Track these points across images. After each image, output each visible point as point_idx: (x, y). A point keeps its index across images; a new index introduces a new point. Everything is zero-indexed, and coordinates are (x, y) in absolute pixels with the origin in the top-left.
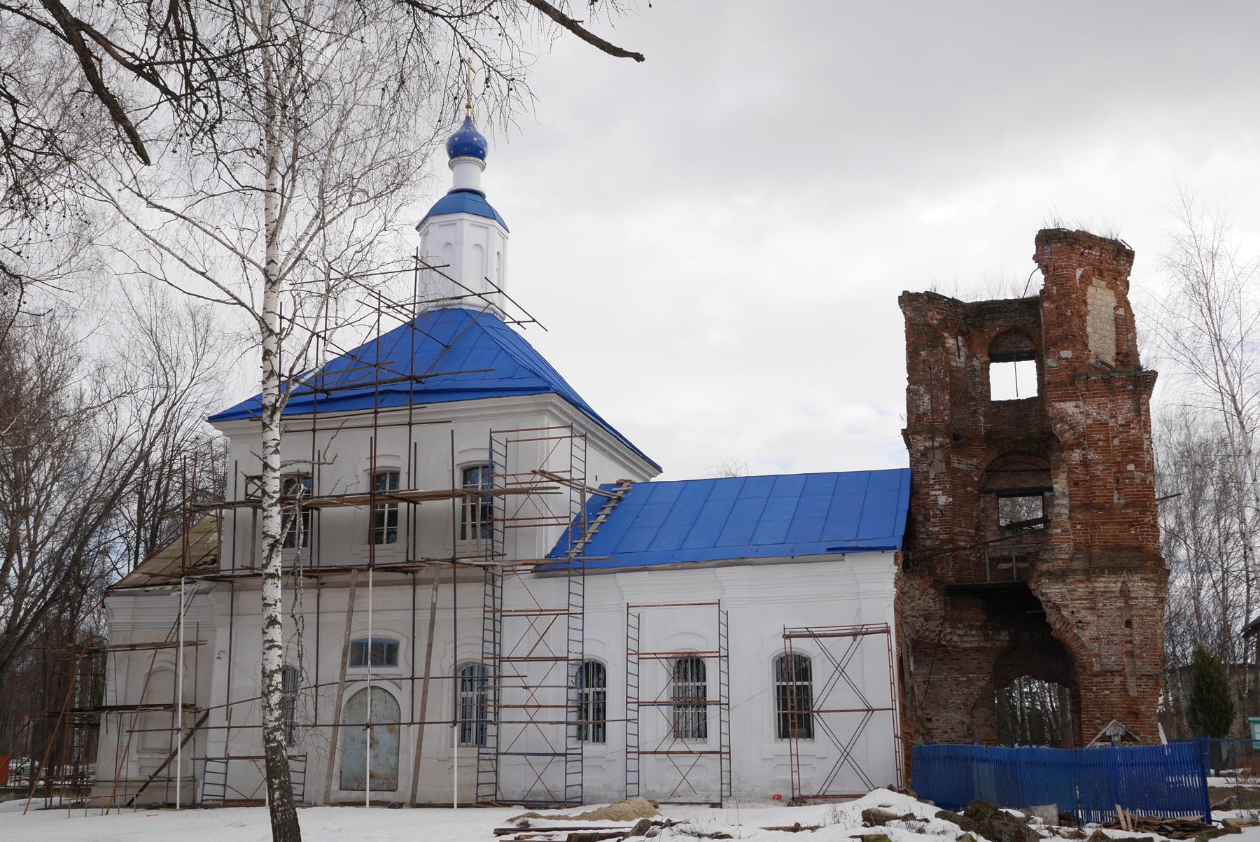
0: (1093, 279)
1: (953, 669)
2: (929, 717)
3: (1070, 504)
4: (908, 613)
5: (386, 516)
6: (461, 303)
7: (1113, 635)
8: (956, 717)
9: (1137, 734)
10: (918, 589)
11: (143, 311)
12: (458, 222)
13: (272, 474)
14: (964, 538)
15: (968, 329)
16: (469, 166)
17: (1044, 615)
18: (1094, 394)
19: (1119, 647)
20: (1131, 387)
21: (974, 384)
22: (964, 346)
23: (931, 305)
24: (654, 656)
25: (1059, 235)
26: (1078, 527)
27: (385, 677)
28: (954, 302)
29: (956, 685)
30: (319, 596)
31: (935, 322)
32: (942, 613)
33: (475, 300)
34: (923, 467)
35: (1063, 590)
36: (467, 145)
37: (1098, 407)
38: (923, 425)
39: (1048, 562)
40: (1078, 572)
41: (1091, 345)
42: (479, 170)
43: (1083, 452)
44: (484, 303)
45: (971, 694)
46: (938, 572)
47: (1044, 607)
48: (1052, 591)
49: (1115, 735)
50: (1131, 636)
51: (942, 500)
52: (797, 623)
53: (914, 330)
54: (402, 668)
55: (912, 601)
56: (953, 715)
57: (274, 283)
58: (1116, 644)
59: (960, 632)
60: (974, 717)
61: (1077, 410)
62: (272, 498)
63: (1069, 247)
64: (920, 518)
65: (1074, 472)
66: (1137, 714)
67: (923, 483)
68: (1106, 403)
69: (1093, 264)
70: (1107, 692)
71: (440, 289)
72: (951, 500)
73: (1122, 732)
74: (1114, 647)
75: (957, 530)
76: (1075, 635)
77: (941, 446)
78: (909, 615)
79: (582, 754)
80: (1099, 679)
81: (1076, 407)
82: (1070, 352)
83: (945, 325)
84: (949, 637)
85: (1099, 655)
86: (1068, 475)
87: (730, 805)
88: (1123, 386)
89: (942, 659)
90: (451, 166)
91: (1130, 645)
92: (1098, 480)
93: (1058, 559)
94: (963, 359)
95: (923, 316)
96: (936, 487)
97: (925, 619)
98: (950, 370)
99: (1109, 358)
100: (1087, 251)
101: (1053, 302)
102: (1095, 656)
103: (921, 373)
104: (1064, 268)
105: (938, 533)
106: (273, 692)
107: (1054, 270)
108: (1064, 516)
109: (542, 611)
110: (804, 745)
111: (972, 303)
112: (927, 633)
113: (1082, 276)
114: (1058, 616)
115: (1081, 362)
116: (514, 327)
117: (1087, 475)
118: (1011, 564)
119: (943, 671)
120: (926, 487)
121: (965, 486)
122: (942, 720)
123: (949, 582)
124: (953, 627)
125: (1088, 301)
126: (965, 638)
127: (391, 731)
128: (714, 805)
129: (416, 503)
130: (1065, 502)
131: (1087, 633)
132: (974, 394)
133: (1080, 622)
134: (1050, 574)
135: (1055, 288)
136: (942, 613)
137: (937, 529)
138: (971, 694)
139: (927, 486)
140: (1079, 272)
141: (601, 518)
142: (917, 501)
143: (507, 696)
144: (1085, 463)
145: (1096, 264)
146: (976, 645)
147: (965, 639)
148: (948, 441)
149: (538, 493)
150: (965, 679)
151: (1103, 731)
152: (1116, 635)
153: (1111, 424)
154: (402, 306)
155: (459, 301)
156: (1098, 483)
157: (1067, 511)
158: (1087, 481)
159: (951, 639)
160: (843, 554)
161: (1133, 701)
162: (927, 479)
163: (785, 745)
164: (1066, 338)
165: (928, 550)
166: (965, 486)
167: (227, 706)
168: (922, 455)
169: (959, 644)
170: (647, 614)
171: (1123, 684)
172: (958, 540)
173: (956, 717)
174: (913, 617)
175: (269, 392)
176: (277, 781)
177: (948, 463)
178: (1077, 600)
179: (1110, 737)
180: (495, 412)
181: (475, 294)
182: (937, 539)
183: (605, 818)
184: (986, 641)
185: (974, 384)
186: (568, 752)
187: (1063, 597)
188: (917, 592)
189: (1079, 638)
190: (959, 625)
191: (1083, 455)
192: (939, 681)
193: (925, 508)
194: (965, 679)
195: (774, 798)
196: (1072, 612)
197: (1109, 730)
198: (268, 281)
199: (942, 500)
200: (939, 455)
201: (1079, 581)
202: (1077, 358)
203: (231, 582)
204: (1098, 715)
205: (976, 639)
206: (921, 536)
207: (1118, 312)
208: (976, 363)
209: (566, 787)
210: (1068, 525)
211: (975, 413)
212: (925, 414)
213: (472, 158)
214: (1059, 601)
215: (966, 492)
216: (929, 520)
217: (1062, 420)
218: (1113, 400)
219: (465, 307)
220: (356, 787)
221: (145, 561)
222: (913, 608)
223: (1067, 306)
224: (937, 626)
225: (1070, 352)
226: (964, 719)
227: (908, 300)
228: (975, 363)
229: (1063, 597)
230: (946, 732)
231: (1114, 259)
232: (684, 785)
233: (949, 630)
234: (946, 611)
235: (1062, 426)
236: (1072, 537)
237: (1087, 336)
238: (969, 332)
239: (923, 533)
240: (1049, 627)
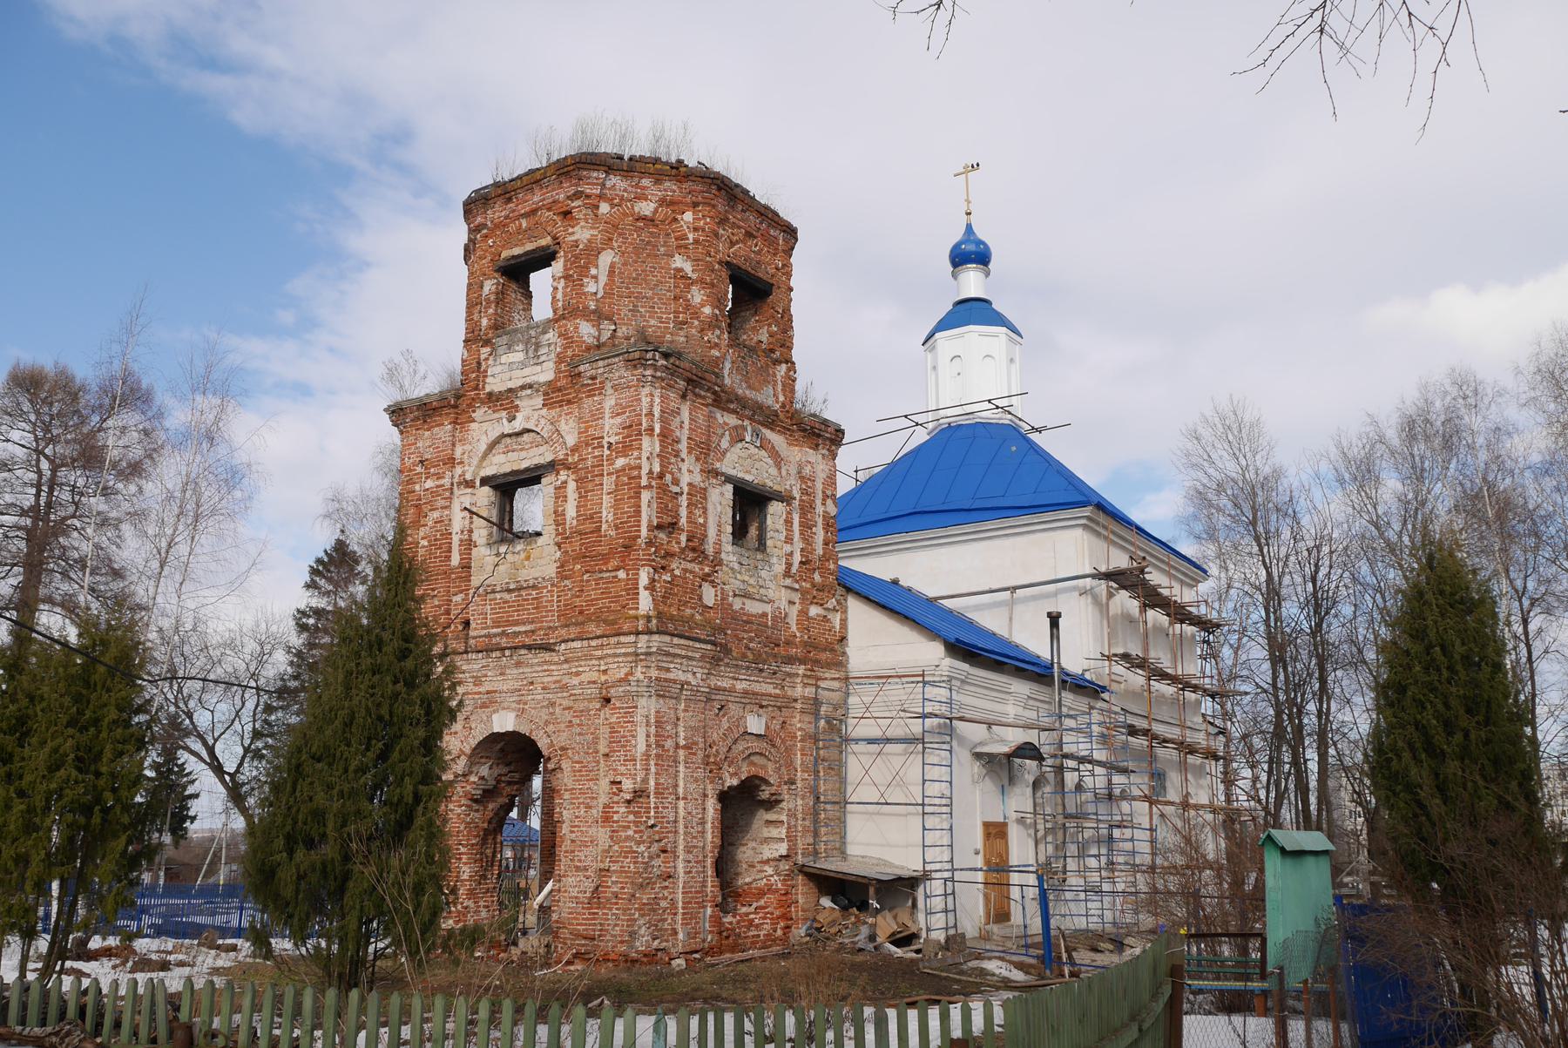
90: (954, 276)
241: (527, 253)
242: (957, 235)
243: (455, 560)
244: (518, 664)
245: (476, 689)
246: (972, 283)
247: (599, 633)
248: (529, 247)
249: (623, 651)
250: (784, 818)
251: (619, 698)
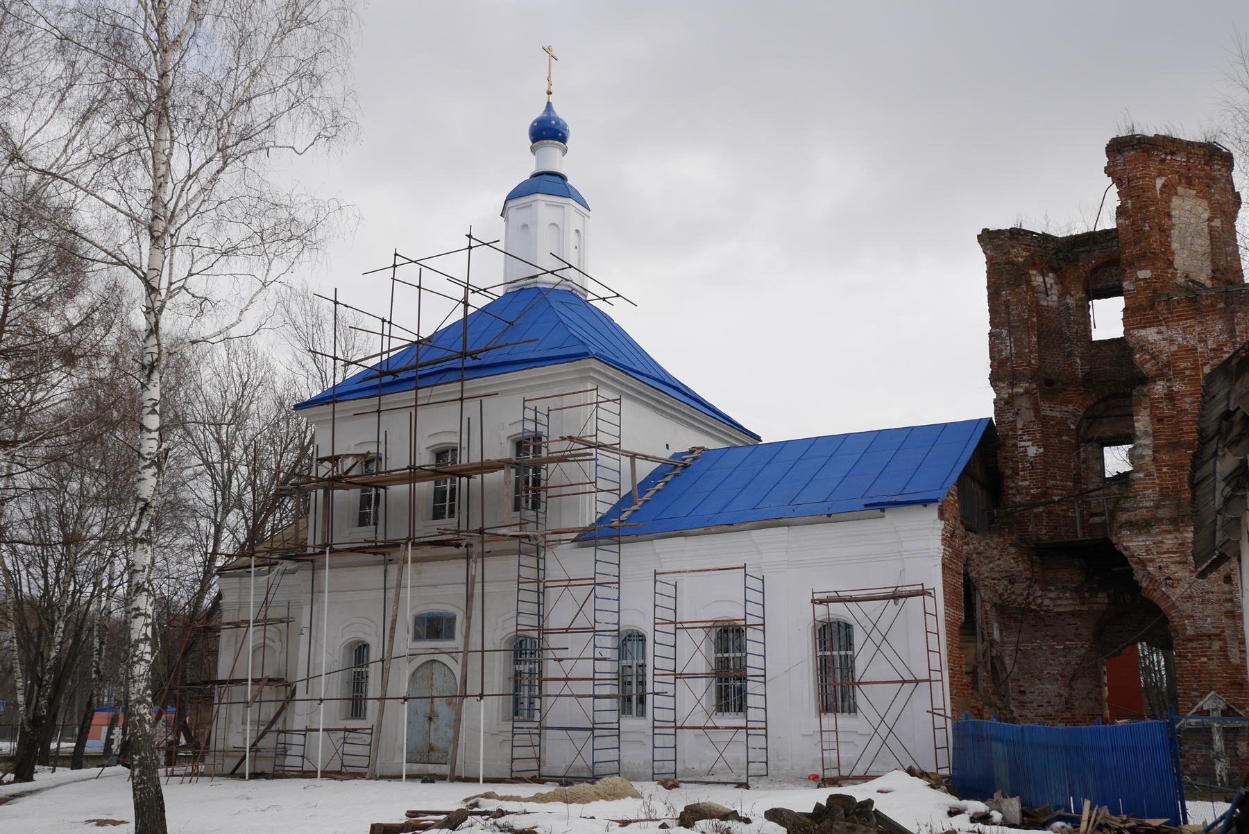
0: (1179, 188)
1: (1047, 636)
2: (1022, 689)
3: (1154, 444)
4: (986, 575)
5: (448, 492)
6: (536, 282)
7: (1208, 593)
8: (1052, 689)
9: (1241, 707)
10: (996, 548)
11: (300, 321)
12: (533, 203)
13: (147, 435)
14: (1060, 492)
15: (1059, 265)
17: (1131, 572)
18: (1177, 316)
19: (1216, 606)
20: (1222, 305)
21: (1068, 324)
22: (1056, 283)
23: (1015, 241)
24: (685, 625)
25: (1132, 141)
26: (1165, 469)
27: (444, 650)
28: (1045, 237)
29: (1052, 654)
30: (386, 571)
31: (1020, 259)
32: (1028, 574)
33: (548, 278)
34: (1009, 416)
35: (1147, 543)
36: (545, 129)
37: (1184, 332)
38: (1007, 371)
39: (1129, 511)
40: (1164, 521)
41: (1178, 262)
42: (561, 153)
43: (1168, 384)
44: (558, 280)
45: (1069, 663)
46: (1030, 530)
47: (1131, 563)
48: (1134, 544)
49: (1214, 710)
50: (1231, 593)
51: (1032, 451)
52: (827, 586)
53: (995, 269)
54: (458, 643)
55: (991, 562)
56: (1050, 687)
57: (158, 238)
58: (1212, 604)
59: (1052, 595)
60: (1074, 690)
61: (1160, 337)
62: (145, 459)
63: (1145, 154)
64: (1008, 472)
65: (1157, 407)
66: (1242, 685)
67: (1010, 433)
68: (1194, 326)
69: (1178, 172)
70: (1205, 659)
71: (522, 271)
72: (1041, 450)
73: (1222, 706)
74: (1210, 607)
75: (1050, 483)
76: (1164, 593)
77: (1027, 392)
78: (987, 577)
79: (619, 729)
80: (1195, 644)
81: (1158, 333)
82: (1149, 271)
83: (1032, 263)
84: (1039, 601)
85: (1192, 617)
86: (1151, 410)
87: (760, 785)
88: (1212, 305)
89: (1035, 626)
90: (533, 150)
91: (1230, 604)
92: (1186, 414)
93: (1141, 508)
94: (1055, 298)
95: (1005, 254)
96: (1026, 437)
97: (1010, 580)
98: (1038, 310)
99: (1204, 277)
100: (1169, 157)
101: (1128, 218)
102: (1189, 617)
103: (1003, 315)
104: (1140, 178)
105: (1028, 488)
106: (137, 662)
107: (1129, 181)
108: (1147, 458)
109: (570, 580)
110: (844, 721)
111: (1067, 237)
112: (1013, 597)
113: (1164, 185)
114: (1145, 573)
115: (1162, 282)
116: (599, 304)
117: (1174, 409)
118: (1103, 518)
119: (1036, 639)
120: (1013, 438)
121: (1059, 435)
122: (1037, 693)
123: (999, 538)
124: (1043, 589)
125: (1173, 213)
126: (1057, 601)
127: (449, 704)
128: (740, 785)
129: (469, 477)
130: (1148, 442)
131: (1178, 591)
132: (1068, 334)
133: (1170, 579)
134: (1131, 525)
135: (1130, 201)
136: (1028, 574)
137: (1026, 483)
138: (1069, 663)
139: (1015, 437)
140: (1159, 183)
141: (659, 486)
142: (1004, 454)
143: (552, 669)
144: (1171, 396)
145: (1183, 171)
146: (1069, 609)
147: (1058, 602)
148: (1035, 386)
149: (577, 461)
150: (1062, 647)
151: (1201, 703)
152: (1212, 593)
153: (1200, 350)
154: (485, 290)
155: (534, 280)
156: (1185, 419)
157: (1150, 452)
158: (1173, 417)
159: (1042, 603)
160: (883, 510)
161: (1236, 669)
162: (1014, 429)
163: (828, 720)
164: (1144, 256)
165: (1018, 507)
166: (1059, 435)
167: (308, 680)
168: (1006, 403)
169: (1051, 608)
170: (686, 582)
171: (1223, 649)
172: (1053, 495)
173: (1052, 689)
174: (994, 579)
175: (148, 350)
176: (137, 758)
177: (1037, 410)
178: (1164, 553)
179: (1208, 711)
181: (548, 272)
182: (1028, 494)
183: (560, 800)
184: (1083, 604)
185: (1068, 324)
186: (596, 726)
187: (1148, 551)
188: (995, 551)
189: (1168, 597)
190: (1052, 588)
191: (1169, 387)
192: (1033, 649)
193: (1012, 461)
194: (1062, 647)
195: (809, 778)
196: (1160, 568)
197: (1207, 703)
198: (152, 237)
199: (1032, 451)
200: (1024, 403)
201: (1166, 531)
202: (1157, 277)
203: (312, 561)
204: (1195, 686)
205: (1071, 602)
206: (1010, 492)
207: (1213, 224)
208: (1070, 301)
209: (748, 762)
210: (1152, 468)
211: (1070, 354)
212: (1008, 359)
213: (550, 141)
214: (1143, 556)
215: (1061, 442)
216: (1018, 474)
217: (1143, 349)
218: (1203, 322)
219: (540, 286)
220: (418, 760)
222: (992, 570)
223: (1144, 220)
224: (1025, 589)
225: (1149, 271)
226: (1062, 692)
227: (988, 239)
228: (1068, 301)
229: (1148, 551)
230: (1042, 706)
231: (1206, 164)
232: (721, 764)
233: (1039, 593)
234: (1033, 572)
235: (1141, 356)
236: (1157, 481)
237: (1173, 254)
238: (1061, 268)
239: (1012, 488)
240: (1136, 586)
242: (538, 112)
246: (553, 158)
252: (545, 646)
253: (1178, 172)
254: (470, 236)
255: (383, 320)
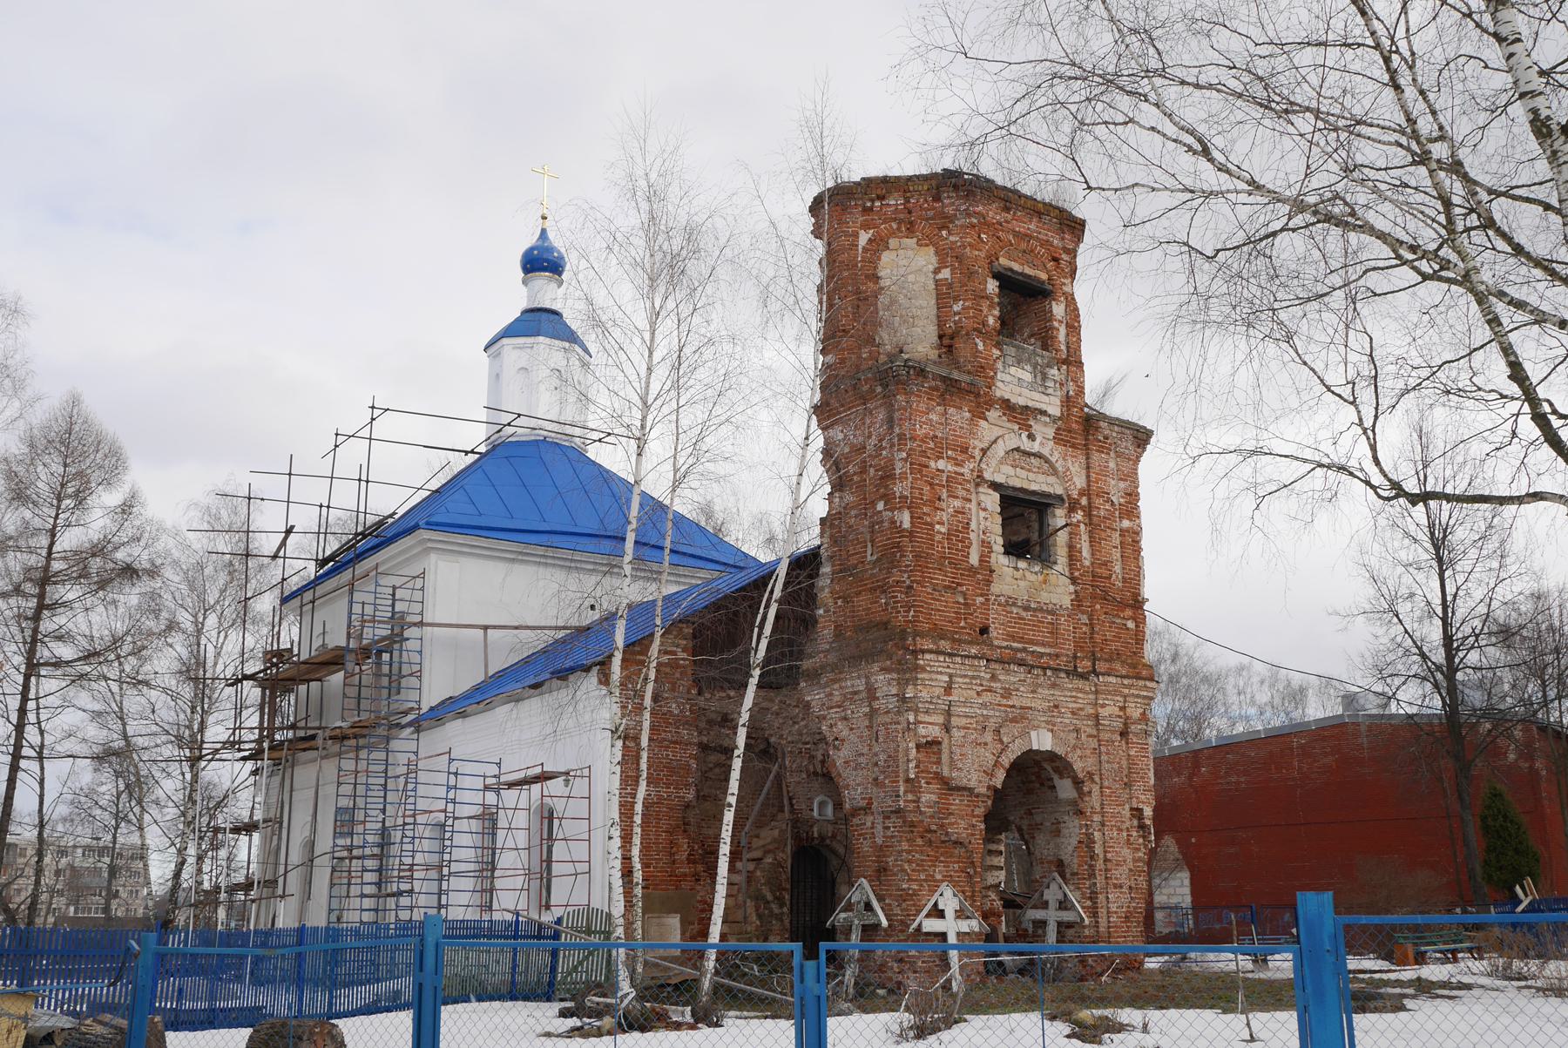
10: (797, 706)
16: (542, 280)
90: (525, 282)
140: (864, 238)
145: (902, 216)
180: (512, 556)
207: (940, 276)
221: (1523, 911)
241: (1021, 274)
242: (529, 240)
243: (974, 559)
244: (1054, 686)
245: (1004, 702)
246: (548, 293)
247: (1124, 672)
248: (1028, 271)
249: (1145, 694)
250: (1002, 848)
251: (1136, 734)
252: (479, 851)
253: (895, 219)
254: (373, 407)
255: (321, 506)
